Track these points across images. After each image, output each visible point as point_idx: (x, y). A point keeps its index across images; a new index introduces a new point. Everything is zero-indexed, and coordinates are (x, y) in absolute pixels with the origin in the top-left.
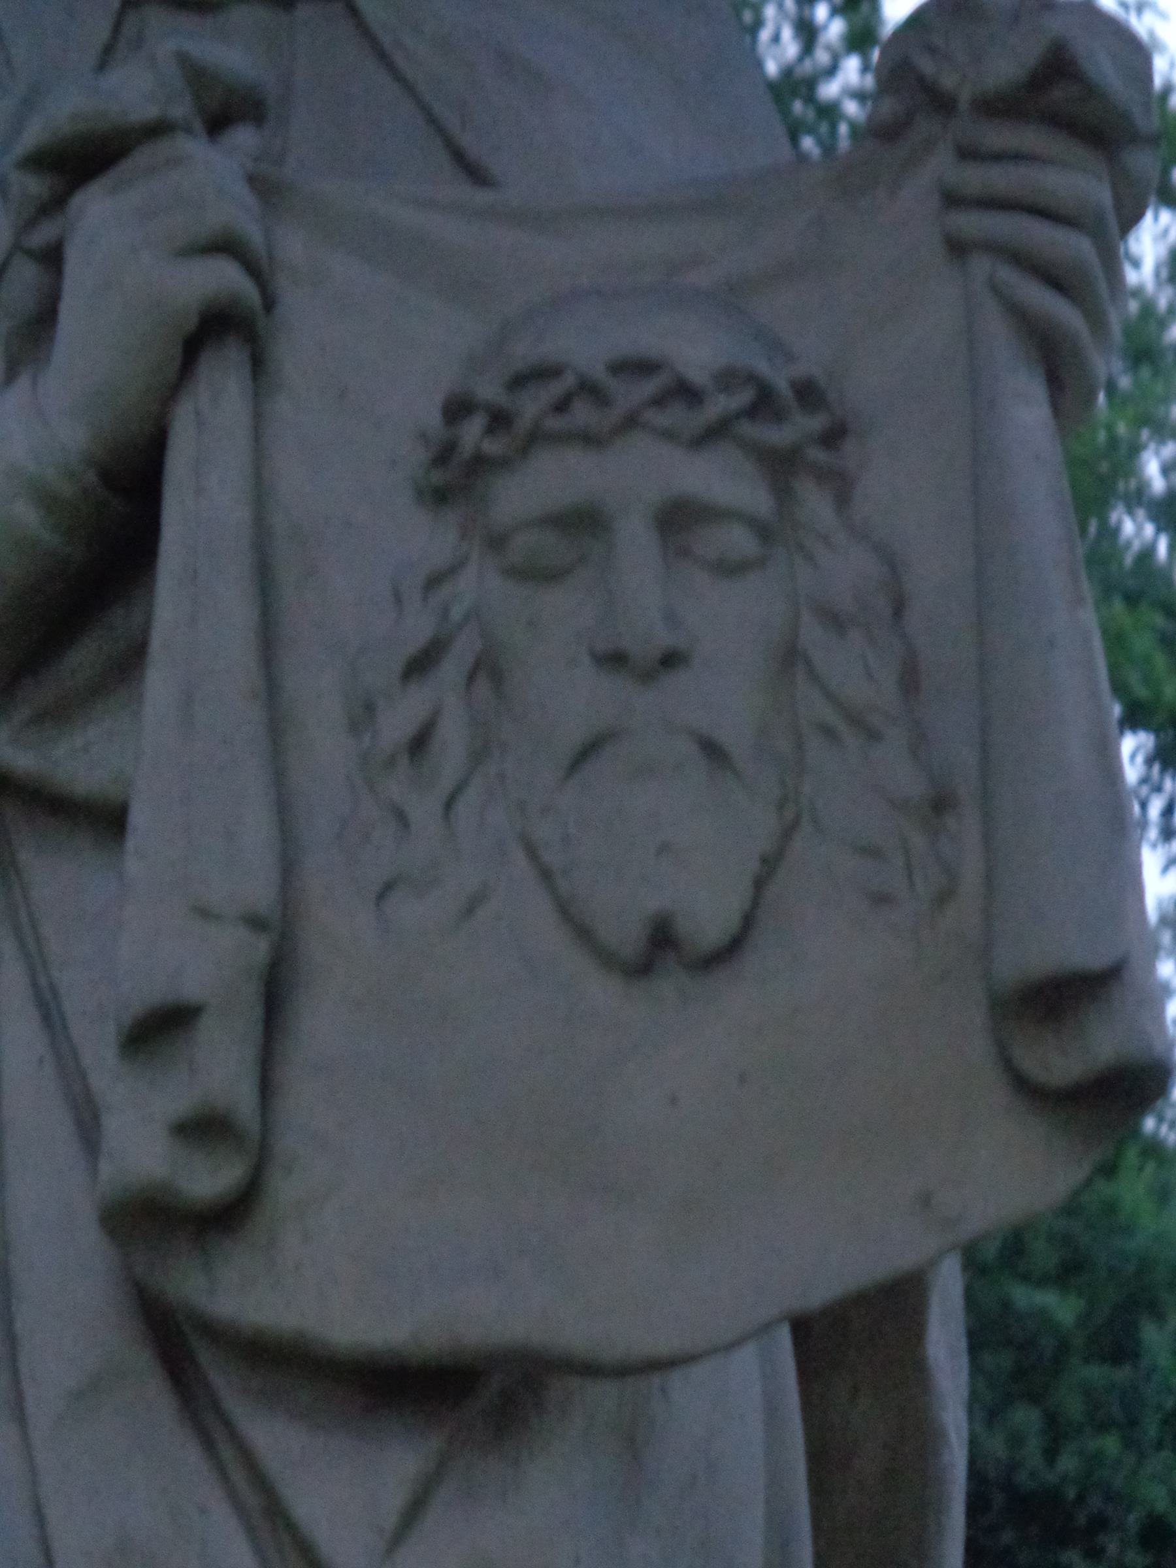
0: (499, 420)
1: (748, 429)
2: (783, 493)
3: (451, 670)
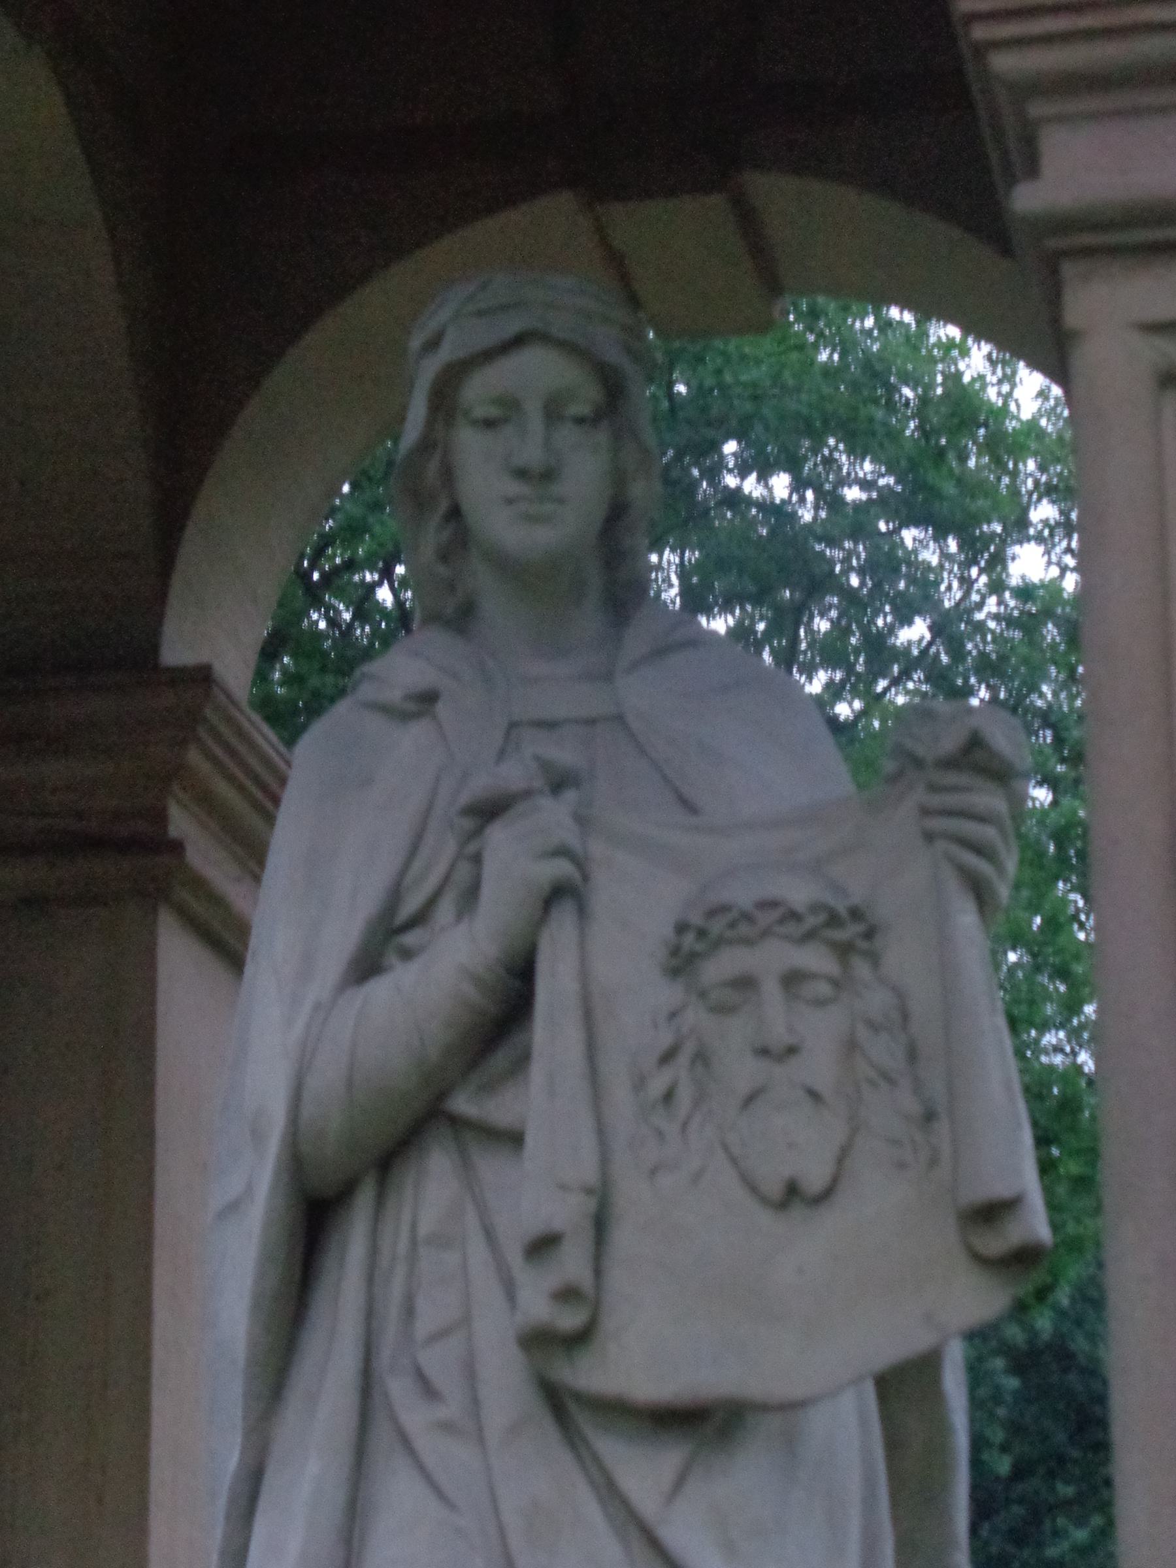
0: (702, 933)
3: (683, 1059)
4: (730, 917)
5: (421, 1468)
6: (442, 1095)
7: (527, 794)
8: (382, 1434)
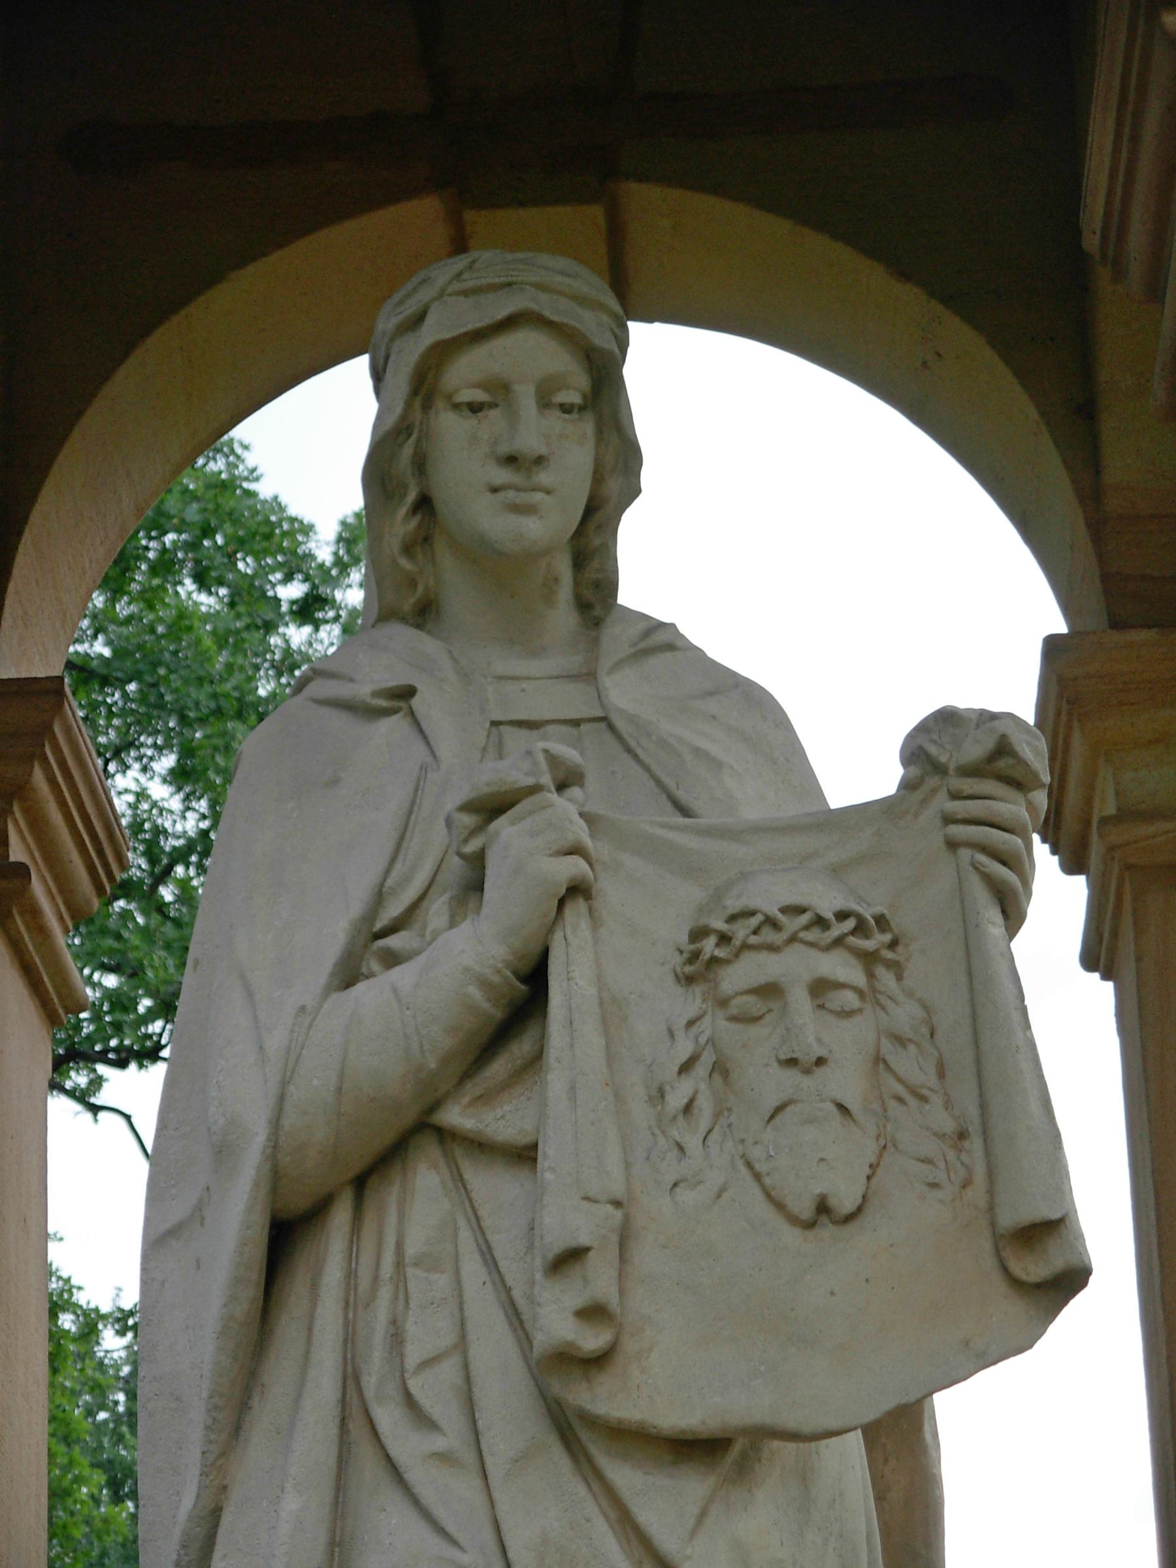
0: (724, 939)
1: (852, 940)
2: (871, 975)
4: (754, 921)
5: (416, 1502)
6: (435, 1106)
7: (535, 789)
8: (364, 1452)
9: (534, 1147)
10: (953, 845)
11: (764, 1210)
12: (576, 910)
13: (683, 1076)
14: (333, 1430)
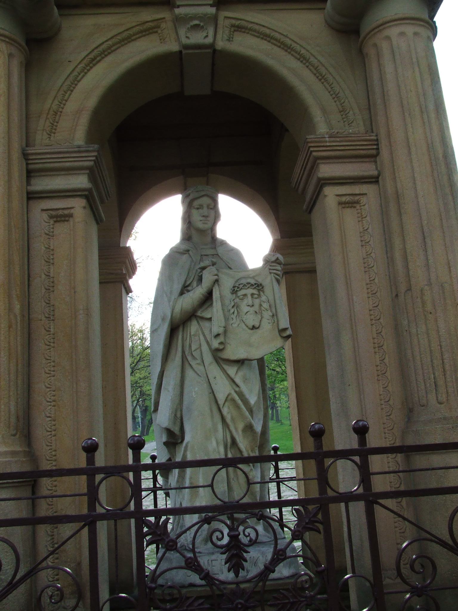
2: (259, 292)
3: (235, 307)
5: (194, 370)
8: (187, 365)
9: (211, 318)
10: (271, 273)
11: (245, 327)
12: (216, 283)
13: (211, 289)
14: (181, 360)
